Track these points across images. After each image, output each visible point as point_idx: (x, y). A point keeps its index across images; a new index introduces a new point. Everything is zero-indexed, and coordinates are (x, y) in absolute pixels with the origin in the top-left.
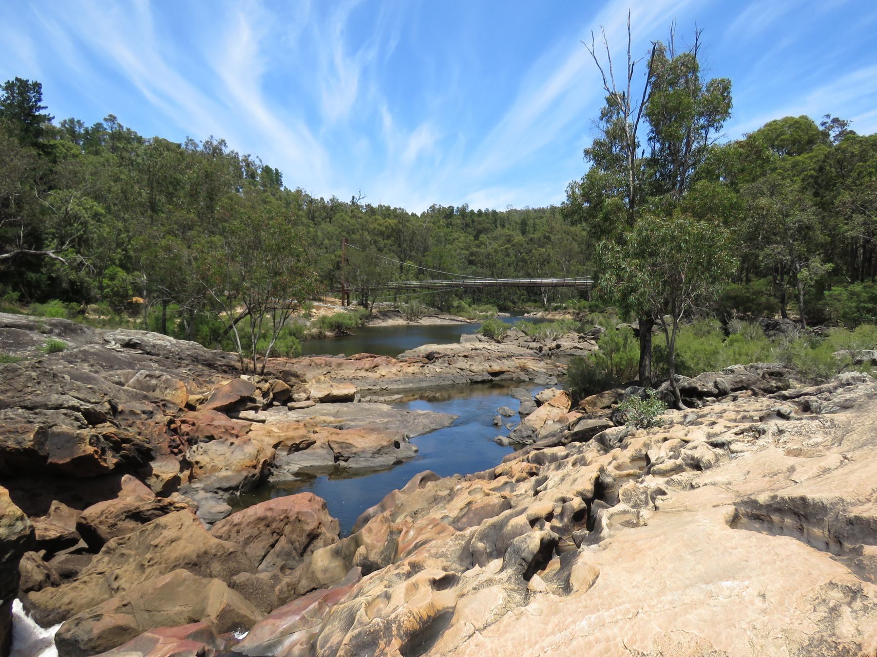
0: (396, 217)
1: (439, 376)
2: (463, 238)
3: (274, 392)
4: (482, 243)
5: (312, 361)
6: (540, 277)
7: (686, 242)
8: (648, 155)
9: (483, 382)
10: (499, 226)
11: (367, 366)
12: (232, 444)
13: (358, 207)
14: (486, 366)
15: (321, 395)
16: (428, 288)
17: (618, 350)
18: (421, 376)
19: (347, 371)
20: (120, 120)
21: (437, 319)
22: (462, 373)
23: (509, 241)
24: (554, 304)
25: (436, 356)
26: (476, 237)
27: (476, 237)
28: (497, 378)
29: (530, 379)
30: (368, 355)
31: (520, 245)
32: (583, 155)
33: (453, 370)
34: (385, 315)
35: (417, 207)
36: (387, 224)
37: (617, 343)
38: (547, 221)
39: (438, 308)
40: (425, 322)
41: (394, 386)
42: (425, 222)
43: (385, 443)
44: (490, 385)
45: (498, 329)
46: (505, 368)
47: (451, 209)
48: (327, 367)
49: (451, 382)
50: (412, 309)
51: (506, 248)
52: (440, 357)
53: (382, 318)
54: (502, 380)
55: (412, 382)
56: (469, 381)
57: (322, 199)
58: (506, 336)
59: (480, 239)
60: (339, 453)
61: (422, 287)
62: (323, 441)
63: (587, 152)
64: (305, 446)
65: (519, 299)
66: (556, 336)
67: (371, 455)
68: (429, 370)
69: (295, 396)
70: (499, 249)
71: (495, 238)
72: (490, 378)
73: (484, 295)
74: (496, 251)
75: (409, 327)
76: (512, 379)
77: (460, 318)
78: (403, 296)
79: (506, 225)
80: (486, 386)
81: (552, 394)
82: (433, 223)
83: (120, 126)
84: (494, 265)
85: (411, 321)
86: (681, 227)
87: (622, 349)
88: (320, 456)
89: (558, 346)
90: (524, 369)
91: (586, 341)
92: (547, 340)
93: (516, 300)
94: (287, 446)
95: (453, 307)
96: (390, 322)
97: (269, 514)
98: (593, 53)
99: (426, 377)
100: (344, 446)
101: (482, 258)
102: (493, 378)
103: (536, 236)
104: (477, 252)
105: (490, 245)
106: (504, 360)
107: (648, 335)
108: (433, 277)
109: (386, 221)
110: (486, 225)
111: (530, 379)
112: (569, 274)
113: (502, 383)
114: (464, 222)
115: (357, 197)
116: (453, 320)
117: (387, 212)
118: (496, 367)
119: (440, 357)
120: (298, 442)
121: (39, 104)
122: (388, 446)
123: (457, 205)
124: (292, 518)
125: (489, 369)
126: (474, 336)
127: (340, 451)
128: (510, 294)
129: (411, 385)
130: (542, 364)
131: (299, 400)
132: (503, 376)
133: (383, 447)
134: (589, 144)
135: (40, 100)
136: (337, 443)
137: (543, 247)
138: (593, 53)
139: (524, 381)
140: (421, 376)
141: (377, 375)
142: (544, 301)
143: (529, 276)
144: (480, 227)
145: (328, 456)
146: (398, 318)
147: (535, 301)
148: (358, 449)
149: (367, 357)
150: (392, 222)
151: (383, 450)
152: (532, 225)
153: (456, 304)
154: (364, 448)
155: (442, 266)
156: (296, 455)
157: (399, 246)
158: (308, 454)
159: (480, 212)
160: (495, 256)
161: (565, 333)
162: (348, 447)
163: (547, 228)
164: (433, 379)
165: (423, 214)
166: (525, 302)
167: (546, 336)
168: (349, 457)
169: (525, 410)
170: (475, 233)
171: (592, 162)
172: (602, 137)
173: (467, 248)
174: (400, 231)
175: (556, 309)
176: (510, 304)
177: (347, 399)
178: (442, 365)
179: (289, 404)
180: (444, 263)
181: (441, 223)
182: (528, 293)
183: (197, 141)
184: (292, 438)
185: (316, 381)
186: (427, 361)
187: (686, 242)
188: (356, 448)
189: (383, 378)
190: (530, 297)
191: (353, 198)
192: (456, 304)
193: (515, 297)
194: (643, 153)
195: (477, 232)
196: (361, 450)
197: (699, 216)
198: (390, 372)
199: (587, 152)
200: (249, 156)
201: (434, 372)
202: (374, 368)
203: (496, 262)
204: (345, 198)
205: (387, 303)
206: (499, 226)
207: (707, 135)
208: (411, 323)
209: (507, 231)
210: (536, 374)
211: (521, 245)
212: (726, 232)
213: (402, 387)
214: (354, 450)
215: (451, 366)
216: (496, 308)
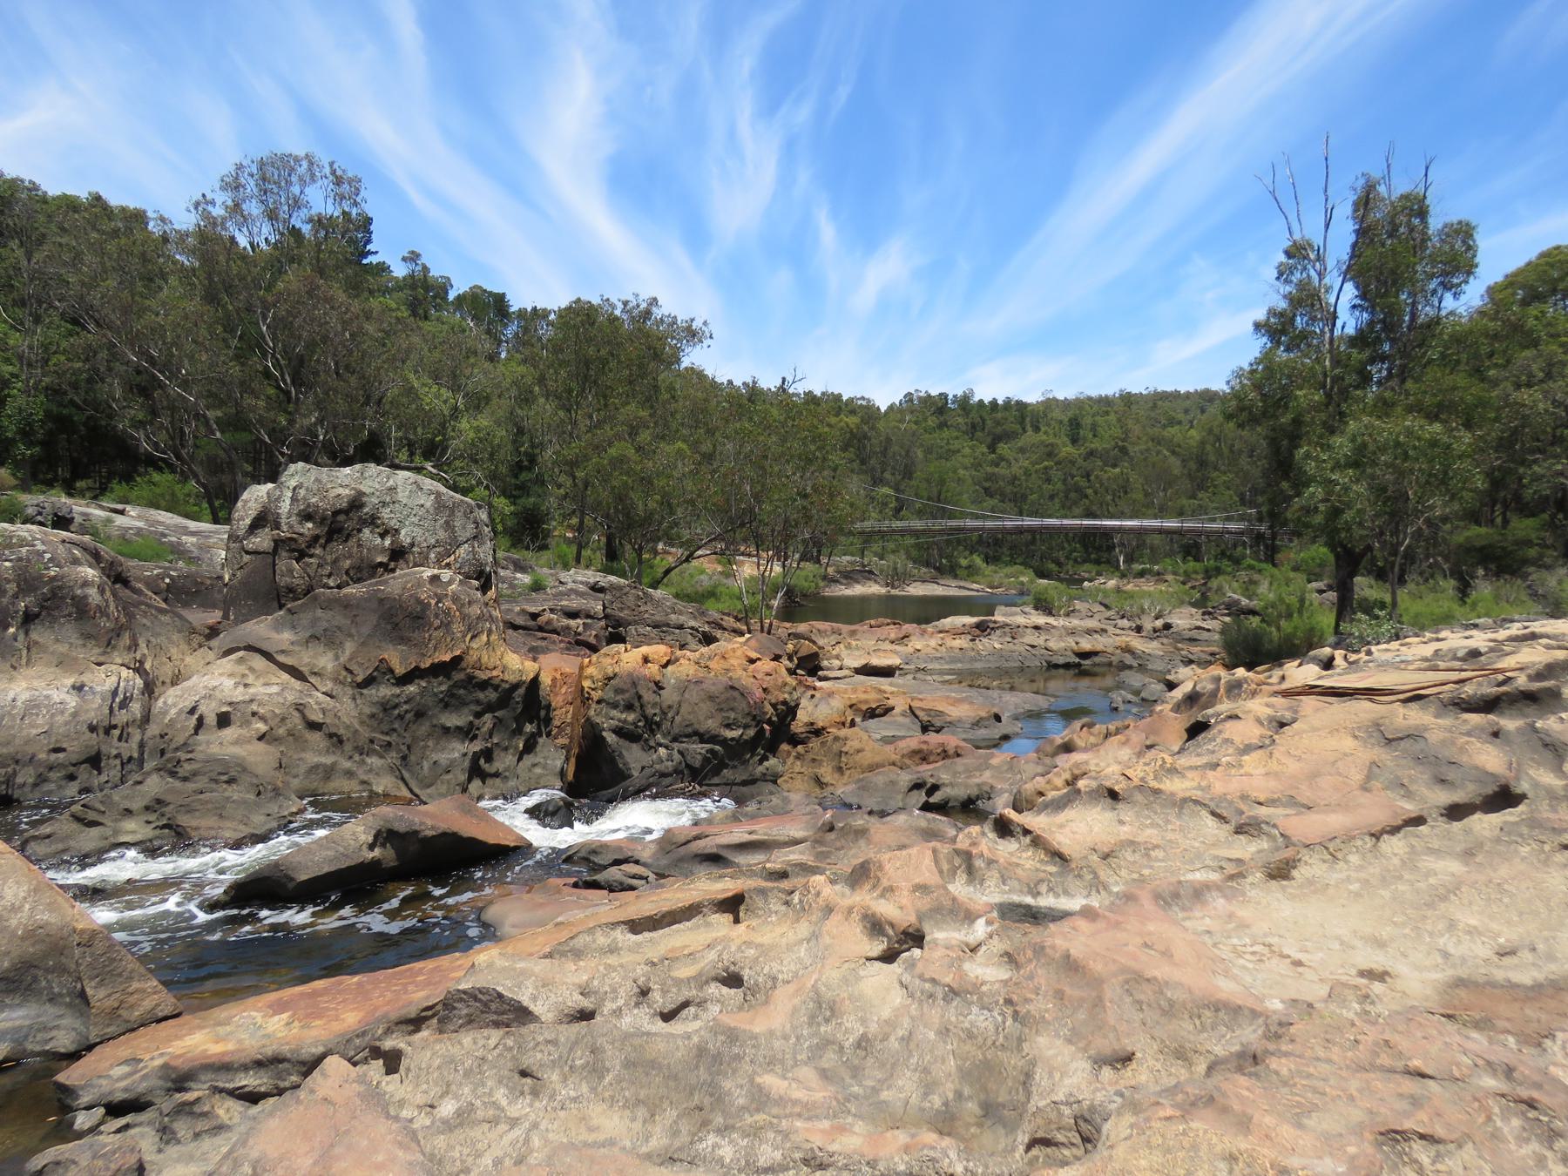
0: (853, 412)
1: (999, 654)
2: (969, 450)
3: (799, 655)
4: (1002, 458)
6: (1112, 517)
8: (1350, 330)
9: (1067, 666)
10: (1028, 428)
11: (893, 636)
12: (813, 696)
14: (1070, 642)
15: (857, 664)
16: (915, 533)
20: (423, 260)
23: (1050, 455)
24: (1137, 567)
25: (991, 625)
26: (992, 448)
27: (992, 448)
31: (1071, 462)
32: (1252, 328)
33: (1019, 647)
34: (849, 576)
35: (885, 397)
36: (842, 424)
37: (1288, 606)
38: (1119, 420)
39: (936, 569)
40: (917, 590)
42: (902, 421)
43: (984, 714)
45: (1060, 599)
46: (1099, 647)
47: (943, 396)
48: (835, 636)
49: (1017, 664)
50: (895, 569)
51: (1046, 468)
54: (1095, 665)
57: (730, 382)
58: (1073, 611)
59: (999, 451)
61: (903, 532)
65: (1068, 558)
66: (1160, 611)
70: (1033, 470)
71: (1022, 450)
72: (1077, 660)
73: (1005, 549)
74: (1027, 473)
75: (889, 598)
77: (975, 586)
78: (876, 547)
80: (1072, 672)
82: (916, 423)
83: (425, 269)
86: (1409, 432)
88: (901, 725)
89: (1167, 626)
90: (1128, 650)
92: (1144, 617)
93: (1062, 560)
96: (858, 590)
97: (924, 747)
98: (1273, 193)
100: (933, 713)
102: (1082, 662)
103: (1096, 445)
104: (994, 474)
105: (1017, 461)
106: (1096, 636)
108: (920, 514)
110: (1009, 427)
112: (1162, 512)
113: (1097, 669)
114: (969, 421)
115: (790, 379)
117: (835, 404)
118: (1086, 645)
121: (368, 247)
122: (987, 719)
123: (954, 389)
124: (951, 752)
125: (1075, 647)
126: (1018, 609)
128: (1051, 549)
129: (959, 665)
130: (1155, 644)
132: (1097, 659)
134: (1260, 314)
135: (369, 241)
136: (923, 710)
137: (1114, 466)
138: (1273, 193)
139: (1130, 667)
141: (910, 649)
142: (1118, 561)
143: (1090, 514)
144: (999, 430)
145: (913, 726)
146: (871, 583)
147: (1098, 562)
150: (853, 421)
153: (964, 562)
155: (942, 497)
156: (872, 723)
157: (863, 462)
159: (994, 403)
160: (1027, 481)
161: (1174, 607)
163: (1117, 432)
164: (991, 658)
165: (891, 408)
167: (1143, 611)
170: (989, 440)
171: (1265, 339)
172: (1282, 305)
173: (977, 466)
174: (865, 437)
175: (1141, 574)
176: (1052, 566)
177: (887, 672)
181: (930, 423)
182: (1085, 547)
183: (614, 300)
184: (866, 702)
186: (978, 632)
187: (1415, 448)
189: (918, 654)
190: (1089, 554)
191: (784, 380)
192: (964, 562)
193: (1061, 555)
194: (1343, 327)
197: (1433, 417)
200: (692, 320)
204: (769, 382)
205: (848, 558)
206: (1028, 428)
208: (895, 592)
209: (1045, 437)
211: (1073, 463)
212: (1467, 437)
213: (947, 667)
214: (948, 719)
216: (1030, 572)
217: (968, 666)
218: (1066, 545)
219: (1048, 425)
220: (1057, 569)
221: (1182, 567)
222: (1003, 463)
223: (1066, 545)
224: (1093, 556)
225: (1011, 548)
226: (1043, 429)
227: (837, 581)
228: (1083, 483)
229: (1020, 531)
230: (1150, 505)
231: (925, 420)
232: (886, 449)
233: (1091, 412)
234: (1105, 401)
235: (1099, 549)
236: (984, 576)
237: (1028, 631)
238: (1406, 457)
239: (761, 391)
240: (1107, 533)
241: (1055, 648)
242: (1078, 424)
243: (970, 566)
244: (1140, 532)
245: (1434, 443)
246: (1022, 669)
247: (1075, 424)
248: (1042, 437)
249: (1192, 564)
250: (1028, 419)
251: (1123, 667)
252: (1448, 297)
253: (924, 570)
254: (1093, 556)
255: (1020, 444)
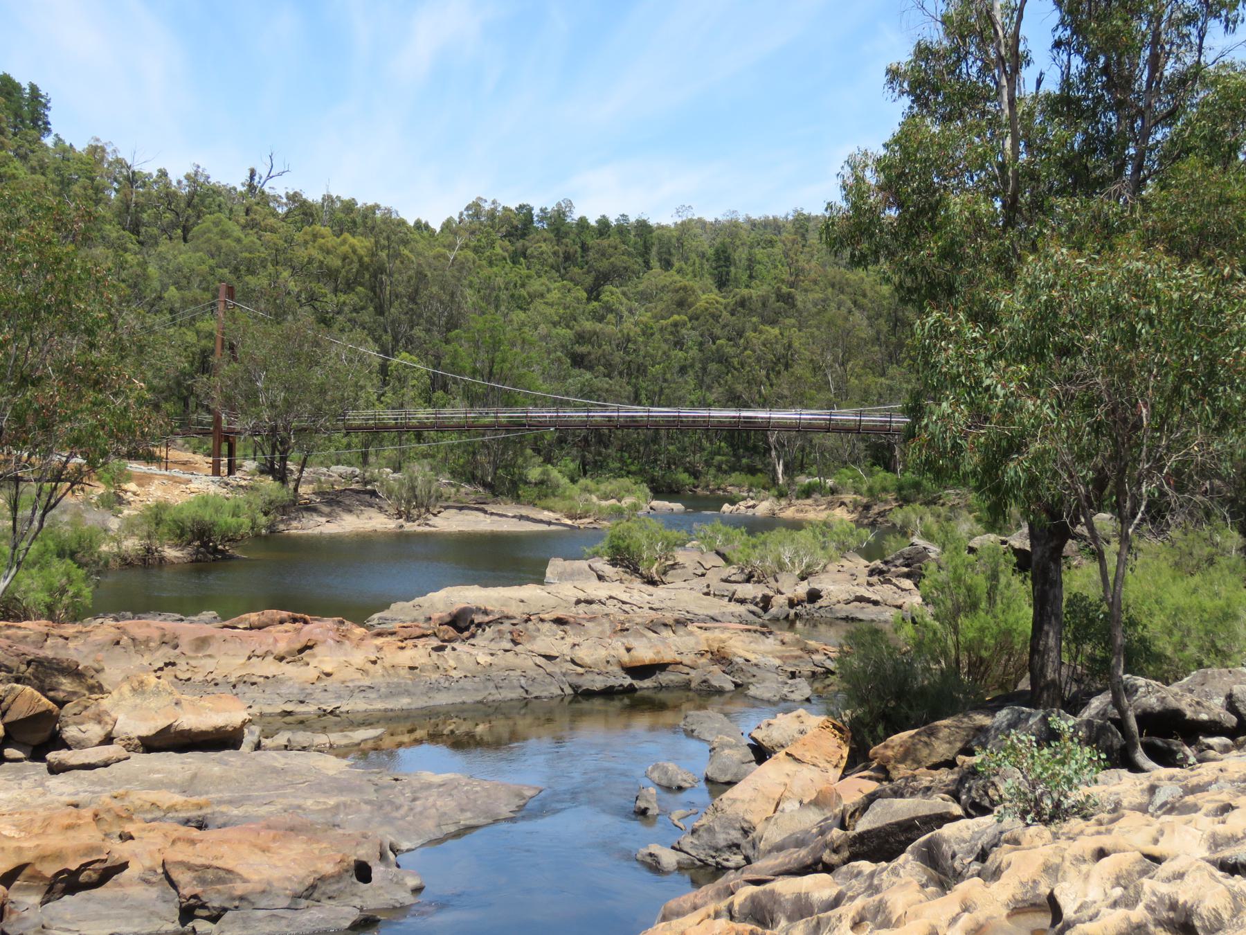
1: (486, 675)
4: (609, 309)
5: (123, 631)
6: (764, 404)
7: (1149, 319)
8: (1052, 86)
9: (609, 693)
10: (654, 262)
11: (282, 647)
13: (265, 199)
14: (617, 647)
15: (147, 728)
17: (974, 606)
18: (435, 676)
19: (223, 660)
21: (481, 515)
22: (550, 667)
23: (681, 304)
24: (803, 480)
25: (478, 618)
26: (594, 293)
27: (594, 293)
28: (647, 683)
29: (737, 685)
30: (284, 614)
31: (713, 316)
32: (884, 79)
33: (524, 660)
34: (335, 501)
36: (345, 248)
37: (969, 589)
39: (485, 485)
40: (450, 522)
41: (358, 705)
42: (451, 247)
43: (329, 868)
44: (626, 701)
45: (651, 546)
46: (668, 656)
47: (526, 211)
49: (517, 694)
50: (413, 488)
51: (675, 325)
52: (489, 623)
53: (326, 509)
54: (660, 688)
55: (408, 693)
56: (569, 691)
57: (163, 174)
58: (673, 567)
60: (195, 896)
62: (148, 863)
63: (894, 75)
64: (95, 876)
65: (708, 464)
66: (808, 566)
67: (286, 903)
68: (458, 659)
69: (70, 732)
70: (656, 327)
71: (645, 297)
72: (628, 681)
75: (402, 538)
76: (686, 686)
77: (547, 515)
78: (389, 451)
79: (674, 260)
80: (617, 704)
81: (796, 726)
82: (476, 250)
84: (642, 370)
85: (408, 519)
86: (1136, 281)
87: (983, 605)
88: (137, 906)
89: (814, 596)
90: (720, 658)
91: (889, 581)
92: (783, 577)
94: (43, 878)
95: (526, 483)
96: (349, 524)
99: (448, 677)
100: (210, 875)
101: (607, 348)
102: (637, 684)
103: (757, 291)
104: (595, 333)
106: (666, 633)
107: (1053, 566)
109: (344, 242)
110: (618, 260)
111: (737, 685)
112: (842, 396)
113: (662, 696)
114: (561, 250)
115: (262, 171)
116: (528, 518)
118: (645, 653)
119: (489, 623)
120: (73, 866)
122: (338, 877)
123: (541, 201)
125: (626, 658)
126: (583, 564)
127: (198, 890)
129: (404, 702)
130: (770, 643)
131: (81, 745)
132: (664, 678)
133: (322, 879)
134: (903, 56)
136: (190, 867)
137: (773, 323)
139: (720, 692)
140: (435, 676)
141: (311, 673)
142: (775, 471)
143: (734, 400)
144: (604, 265)
145: (163, 908)
146: (373, 512)
147: (752, 471)
148: (249, 886)
149: (282, 622)
150: (361, 243)
151: (323, 888)
152: (745, 263)
153: (534, 474)
154: (269, 883)
155: (496, 368)
157: (380, 310)
158: (102, 902)
159: (604, 223)
161: (831, 559)
162: (221, 881)
165: (447, 225)
166: (725, 472)
167: (781, 566)
168: (225, 910)
169: (724, 771)
170: (589, 280)
172: (936, 36)
173: (568, 320)
174: (382, 270)
175: (807, 492)
176: (684, 477)
178: (493, 646)
179: (52, 756)
180: (504, 361)
181: (498, 250)
184: (58, 856)
185: (134, 690)
186: (452, 632)
187: (1149, 319)
188: (245, 881)
190: (739, 458)
191: (253, 174)
192: (534, 474)
193: (697, 459)
194: (1039, 82)
195: (597, 279)
196: (259, 888)
198: (348, 664)
199: (894, 75)
201: (472, 666)
202: (301, 651)
203: (648, 361)
205: (342, 469)
206: (654, 262)
207: (1201, 39)
208: (410, 527)
209: (678, 277)
210: (754, 670)
211: (716, 317)
213: (379, 705)
214: (239, 888)
215: (519, 648)
217: (421, 702)
218: (706, 443)
219: (686, 260)
220: (692, 480)
221: (867, 482)
222: (610, 317)
223: (706, 443)
224: (744, 461)
225: (621, 450)
226: (677, 265)
227: (314, 510)
228: (729, 350)
229: (633, 424)
230: (823, 387)
231: (492, 245)
232: (416, 291)
233: (748, 241)
234: (774, 226)
235: (755, 450)
236: (564, 498)
237: (546, 627)
238: (1132, 338)
239: (216, 191)
240: (764, 428)
241: (588, 660)
242: (727, 259)
243: (542, 482)
244: (803, 429)
245: (1187, 310)
246: (526, 702)
247: (723, 258)
248: (672, 277)
249: (881, 475)
250: (654, 250)
251: (709, 693)
252: (1215, 26)
253: (467, 488)
254: (744, 461)
255: (641, 287)
